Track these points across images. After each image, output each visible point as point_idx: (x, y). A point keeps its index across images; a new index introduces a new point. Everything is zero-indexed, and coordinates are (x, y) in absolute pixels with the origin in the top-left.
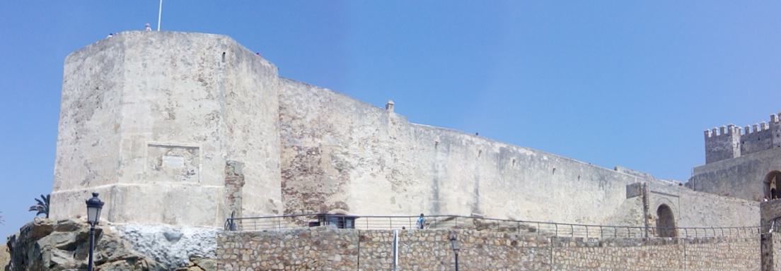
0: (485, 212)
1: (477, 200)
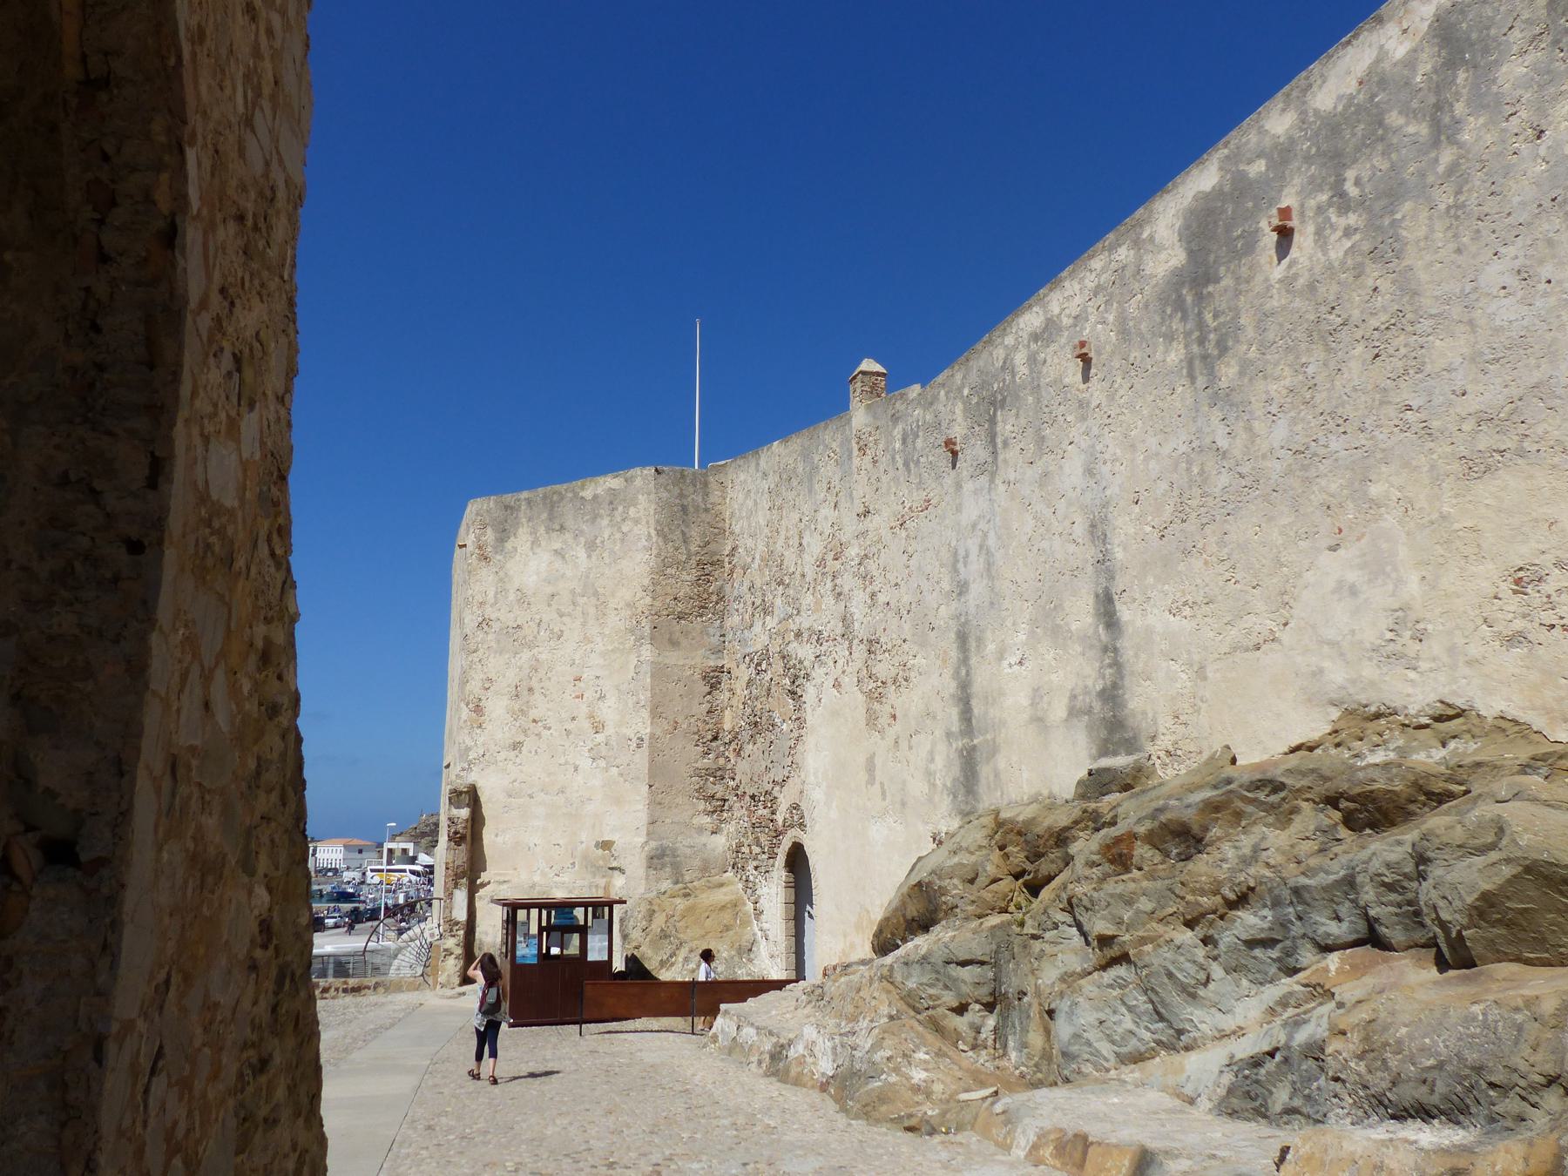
0: (1164, 722)
1: (1117, 665)
